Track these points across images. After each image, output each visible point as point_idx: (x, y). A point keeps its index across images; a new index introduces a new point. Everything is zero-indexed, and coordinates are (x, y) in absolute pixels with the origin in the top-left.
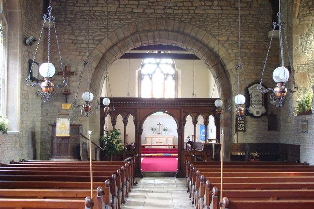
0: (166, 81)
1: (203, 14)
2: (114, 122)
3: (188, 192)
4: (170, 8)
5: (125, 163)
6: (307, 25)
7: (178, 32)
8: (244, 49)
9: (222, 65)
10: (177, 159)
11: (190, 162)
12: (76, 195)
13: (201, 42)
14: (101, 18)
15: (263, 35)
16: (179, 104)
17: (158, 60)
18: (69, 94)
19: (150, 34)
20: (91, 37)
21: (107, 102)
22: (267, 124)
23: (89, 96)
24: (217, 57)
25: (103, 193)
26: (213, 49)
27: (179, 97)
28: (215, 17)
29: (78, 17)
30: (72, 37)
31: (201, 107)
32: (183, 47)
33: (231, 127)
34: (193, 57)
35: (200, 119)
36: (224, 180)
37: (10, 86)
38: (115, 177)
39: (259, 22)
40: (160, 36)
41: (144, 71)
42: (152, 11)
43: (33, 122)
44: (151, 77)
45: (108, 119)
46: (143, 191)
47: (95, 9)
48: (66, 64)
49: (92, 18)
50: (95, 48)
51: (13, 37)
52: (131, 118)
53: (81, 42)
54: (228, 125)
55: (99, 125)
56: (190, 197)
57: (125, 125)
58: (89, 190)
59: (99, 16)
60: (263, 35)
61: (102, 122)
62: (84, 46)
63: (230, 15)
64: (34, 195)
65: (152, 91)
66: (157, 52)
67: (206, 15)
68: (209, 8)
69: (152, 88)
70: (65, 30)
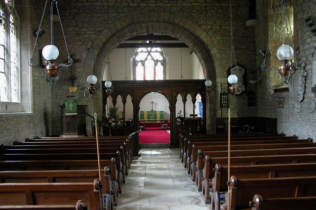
1: (189, 6)
2: (114, 102)
3: (182, 162)
5: (125, 139)
6: (281, 14)
7: (168, 22)
8: (225, 36)
9: (207, 50)
10: (169, 132)
11: (183, 136)
12: (85, 175)
13: (188, 31)
14: (101, 12)
15: (242, 24)
16: (173, 85)
17: (149, 49)
18: (75, 78)
19: (144, 25)
20: (93, 29)
21: (108, 84)
23: (94, 79)
24: (203, 43)
25: (110, 172)
26: (199, 37)
27: (167, 79)
28: (200, 9)
29: (81, 11)
30: (76, 29)
31: (190, 87)
32: (173, 36)
33: (215, 104)
34: (183, 45)
35: (189, 97)
36: (232, 162)
37: (23, 72)
38: (119, 153)
39: (238, 13)
40: (153, 26)
41: (138, 58)
42: (145, 5)
43: (45, 104)
44: (143, 63)
45: (109, 100)
46: (142, 162)
47: (96, 4)
48: (72, 53)
49: (93, 12)
50: (96, 38)
51: (24, 30)
52: (129, 98)
53: (84, 33)
54: (213, 102)
55: (102, 105)
56: (185, 167)
57: (124, 105)
58: (97, 170)
59: (99, 10)
60: (242, 24)
61: (105, 102)
62: (87, 36)
63: (213, 7)
64: (44, 176)
65: (144, 75)
66: (148, 42)
67: (192, 7)
69: (145, 73)
70: (70, 22)
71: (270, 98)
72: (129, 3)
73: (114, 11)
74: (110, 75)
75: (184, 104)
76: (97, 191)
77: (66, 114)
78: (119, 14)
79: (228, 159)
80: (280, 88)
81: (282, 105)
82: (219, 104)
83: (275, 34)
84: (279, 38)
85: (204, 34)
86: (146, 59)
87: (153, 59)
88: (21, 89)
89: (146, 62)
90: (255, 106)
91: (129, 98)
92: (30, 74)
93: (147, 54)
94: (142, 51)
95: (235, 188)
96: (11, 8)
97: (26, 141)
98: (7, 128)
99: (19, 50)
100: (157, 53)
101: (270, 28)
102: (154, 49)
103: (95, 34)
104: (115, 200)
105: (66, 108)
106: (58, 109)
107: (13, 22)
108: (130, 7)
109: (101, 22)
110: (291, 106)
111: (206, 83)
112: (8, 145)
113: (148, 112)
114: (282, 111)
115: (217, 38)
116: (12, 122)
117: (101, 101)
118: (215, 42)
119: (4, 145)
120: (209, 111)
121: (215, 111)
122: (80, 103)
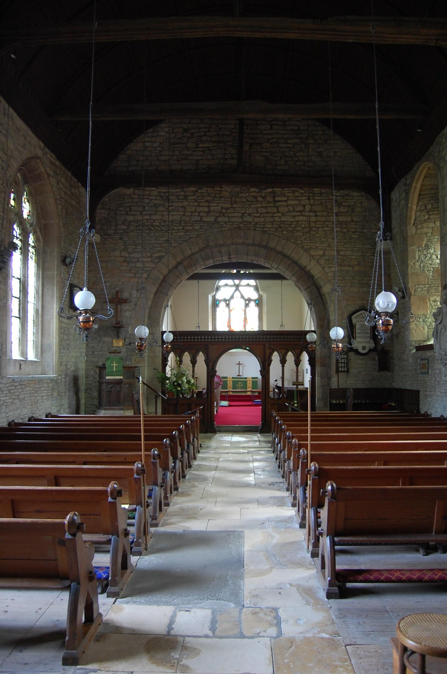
0: (248, 309)
1: (292, 222)
4: (250, 215)
6: (426, 234)
7: (259, 245)
9: (317, 287)
11: (274, 413)
12: (125, 459)
13: (289, 258)
14: (162, 230)
15: (371, 247)
17: (237, 282)
18: (122, 327)
19: (223, 249)
22: (377, 362)
26: (306, 267)
30: (124, 254)
32: (266, 265)
35: (290, 357)
37: (46, 317)
39: (365, 231)
41: (220, 295)
42: (226, 219)
44: (227, 302)
47: (153, 217)
49: (150, 230)
50: (154, 268)
52: (201, 358)
54: (326, 365)
57: (194, 367)
59: (158, 226)
63: (326, 223)
66: (235, 271)
68: (299, 214)
70: (115, 245)
71: (411, 360)
72: (202, 217)
73: (181, 228)
74: (174, 321)
75: (283, 366)
76: (138, 477)
77: (107, 378)
78: (187, 233)
79: (308, 436)
80: (425, 344)
81: (426, 370)
82: (335, 367)
83: (417, 264)
84: (423, 270)
85: (313, 263)
86: (232, 297)
87: (242, 297)
88: (42, 342)
89: (232, 303)
90: (389, 371)
91: (201, 358)
92: (55, 320)
93: (234, 288)
94: (226, 285)
95: (317, 477)
96: (31, 225)
97: (47, 416)
98: (21, 397)
99: (41, 285)
100: (248, 288)
101: (410, 255)
102: (244, 282)
103: (152, 261)
104: (166, 498)
105: (108, 370)
106: (95, 371)
107: (33, 244)
108: (205, 222)
109: (161, 244)
110: (437, 371)
111: (308, 336)
112: (21, 421)
113: (233, 378)
114: (426, 378)
115: (332, 269)
116: (27, 389)
117: (159, 360)
118: (330, 274)
119: (16, 421)
120: (319, 378)
121: (329, 379)
122: (127, 363)
